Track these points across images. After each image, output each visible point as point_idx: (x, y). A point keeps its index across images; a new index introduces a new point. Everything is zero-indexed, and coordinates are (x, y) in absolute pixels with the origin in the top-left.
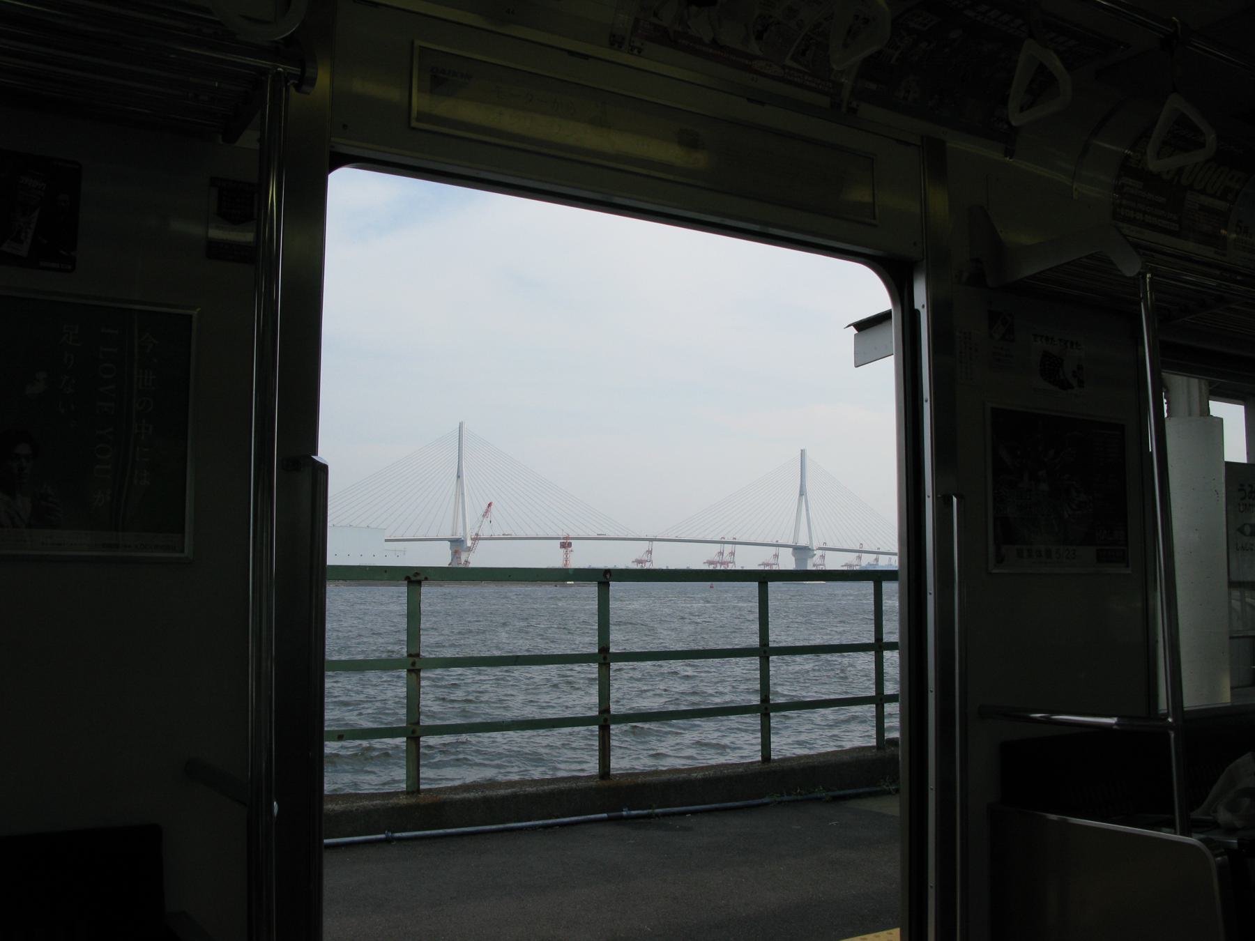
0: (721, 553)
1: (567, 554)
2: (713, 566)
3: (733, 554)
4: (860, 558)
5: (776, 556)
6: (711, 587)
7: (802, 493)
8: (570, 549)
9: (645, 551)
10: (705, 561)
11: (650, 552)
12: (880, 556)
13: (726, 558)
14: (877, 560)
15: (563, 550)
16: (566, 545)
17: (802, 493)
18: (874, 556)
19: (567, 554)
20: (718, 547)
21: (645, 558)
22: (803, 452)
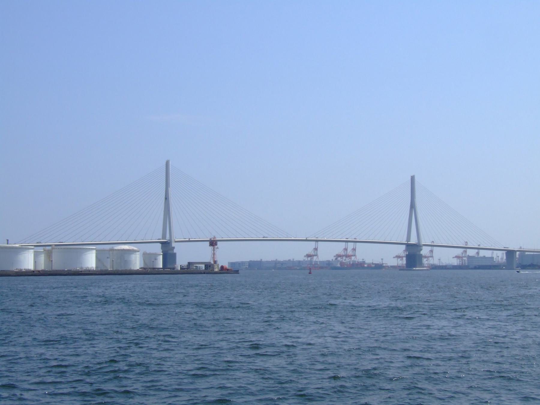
0: (346, 249)
1: (214, 250)
2: (310, 258)
3: (354, 250)
4: (465, 252)
5: (316, 249)
6: (310, 273)
7: (413, 206)
8: (216, 247)
9: (343, 249)
10: (395, 256)
11: (316, 249)
12: (434, 248)
13: (350, 252)
14: (478, 253)
15: (212, 248)
16: (213, 243)
17: (413, 206)
18: (476, 251)
19: (214, 250)
20: (343, 245)
21: (313, 253)
22: (413, 178)
